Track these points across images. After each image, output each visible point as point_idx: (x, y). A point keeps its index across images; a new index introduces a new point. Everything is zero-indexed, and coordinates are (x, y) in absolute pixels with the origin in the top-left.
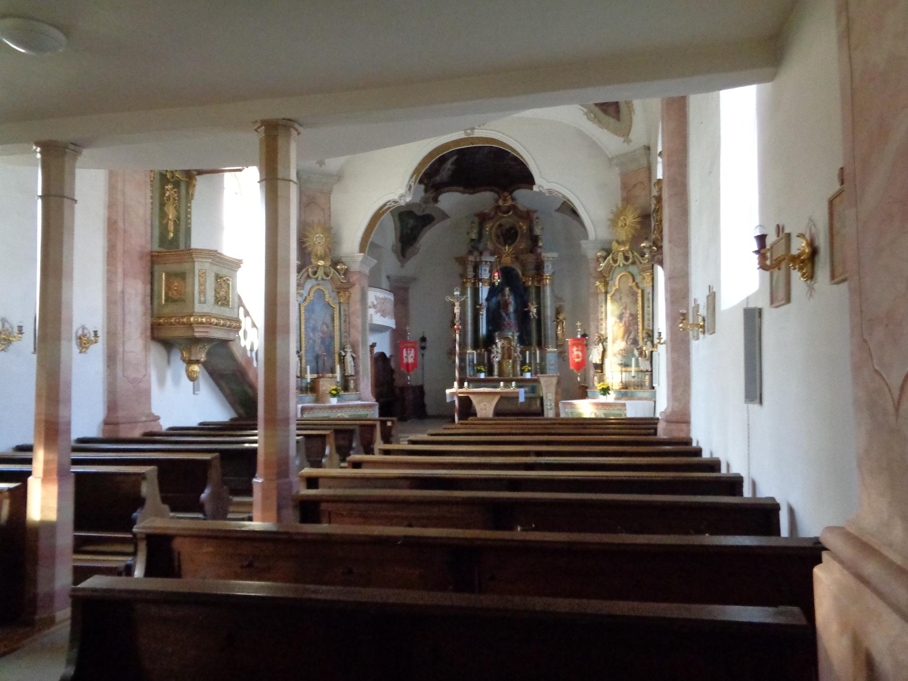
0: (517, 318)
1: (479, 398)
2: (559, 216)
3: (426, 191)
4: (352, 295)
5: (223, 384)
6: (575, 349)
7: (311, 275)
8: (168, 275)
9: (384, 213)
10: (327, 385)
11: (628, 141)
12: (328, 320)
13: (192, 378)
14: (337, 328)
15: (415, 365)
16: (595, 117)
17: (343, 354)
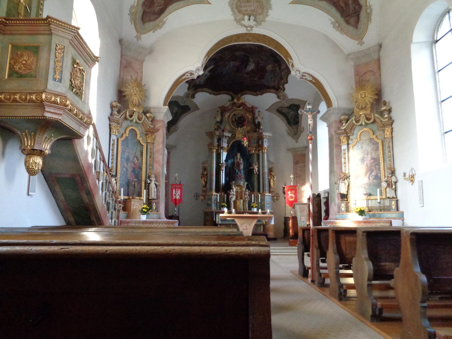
0: (245, 173)
1: (243, 221)
2: (267, 113)
3: (189, 89)
4: (157, 138)
5: (58, 189)
6: (289, 192)
7: (128, 116)
8: (15, 47)
9: (181, 82)
10: (137, 204)
11: (361, 43)
12: (138, 154)
13: (31, 172)
14: (144, 161)
15: (180, 200)
16: (339, 26)
17: (149, 182)
